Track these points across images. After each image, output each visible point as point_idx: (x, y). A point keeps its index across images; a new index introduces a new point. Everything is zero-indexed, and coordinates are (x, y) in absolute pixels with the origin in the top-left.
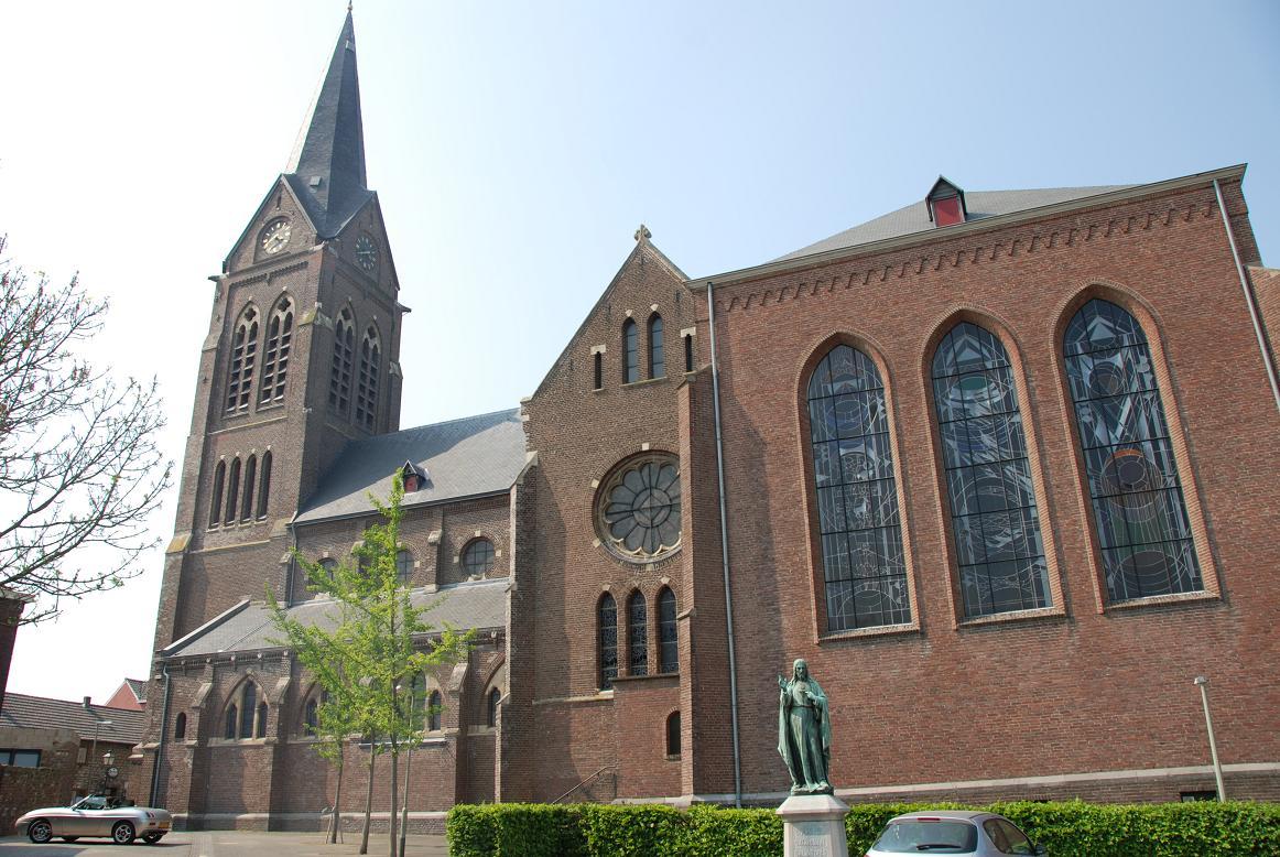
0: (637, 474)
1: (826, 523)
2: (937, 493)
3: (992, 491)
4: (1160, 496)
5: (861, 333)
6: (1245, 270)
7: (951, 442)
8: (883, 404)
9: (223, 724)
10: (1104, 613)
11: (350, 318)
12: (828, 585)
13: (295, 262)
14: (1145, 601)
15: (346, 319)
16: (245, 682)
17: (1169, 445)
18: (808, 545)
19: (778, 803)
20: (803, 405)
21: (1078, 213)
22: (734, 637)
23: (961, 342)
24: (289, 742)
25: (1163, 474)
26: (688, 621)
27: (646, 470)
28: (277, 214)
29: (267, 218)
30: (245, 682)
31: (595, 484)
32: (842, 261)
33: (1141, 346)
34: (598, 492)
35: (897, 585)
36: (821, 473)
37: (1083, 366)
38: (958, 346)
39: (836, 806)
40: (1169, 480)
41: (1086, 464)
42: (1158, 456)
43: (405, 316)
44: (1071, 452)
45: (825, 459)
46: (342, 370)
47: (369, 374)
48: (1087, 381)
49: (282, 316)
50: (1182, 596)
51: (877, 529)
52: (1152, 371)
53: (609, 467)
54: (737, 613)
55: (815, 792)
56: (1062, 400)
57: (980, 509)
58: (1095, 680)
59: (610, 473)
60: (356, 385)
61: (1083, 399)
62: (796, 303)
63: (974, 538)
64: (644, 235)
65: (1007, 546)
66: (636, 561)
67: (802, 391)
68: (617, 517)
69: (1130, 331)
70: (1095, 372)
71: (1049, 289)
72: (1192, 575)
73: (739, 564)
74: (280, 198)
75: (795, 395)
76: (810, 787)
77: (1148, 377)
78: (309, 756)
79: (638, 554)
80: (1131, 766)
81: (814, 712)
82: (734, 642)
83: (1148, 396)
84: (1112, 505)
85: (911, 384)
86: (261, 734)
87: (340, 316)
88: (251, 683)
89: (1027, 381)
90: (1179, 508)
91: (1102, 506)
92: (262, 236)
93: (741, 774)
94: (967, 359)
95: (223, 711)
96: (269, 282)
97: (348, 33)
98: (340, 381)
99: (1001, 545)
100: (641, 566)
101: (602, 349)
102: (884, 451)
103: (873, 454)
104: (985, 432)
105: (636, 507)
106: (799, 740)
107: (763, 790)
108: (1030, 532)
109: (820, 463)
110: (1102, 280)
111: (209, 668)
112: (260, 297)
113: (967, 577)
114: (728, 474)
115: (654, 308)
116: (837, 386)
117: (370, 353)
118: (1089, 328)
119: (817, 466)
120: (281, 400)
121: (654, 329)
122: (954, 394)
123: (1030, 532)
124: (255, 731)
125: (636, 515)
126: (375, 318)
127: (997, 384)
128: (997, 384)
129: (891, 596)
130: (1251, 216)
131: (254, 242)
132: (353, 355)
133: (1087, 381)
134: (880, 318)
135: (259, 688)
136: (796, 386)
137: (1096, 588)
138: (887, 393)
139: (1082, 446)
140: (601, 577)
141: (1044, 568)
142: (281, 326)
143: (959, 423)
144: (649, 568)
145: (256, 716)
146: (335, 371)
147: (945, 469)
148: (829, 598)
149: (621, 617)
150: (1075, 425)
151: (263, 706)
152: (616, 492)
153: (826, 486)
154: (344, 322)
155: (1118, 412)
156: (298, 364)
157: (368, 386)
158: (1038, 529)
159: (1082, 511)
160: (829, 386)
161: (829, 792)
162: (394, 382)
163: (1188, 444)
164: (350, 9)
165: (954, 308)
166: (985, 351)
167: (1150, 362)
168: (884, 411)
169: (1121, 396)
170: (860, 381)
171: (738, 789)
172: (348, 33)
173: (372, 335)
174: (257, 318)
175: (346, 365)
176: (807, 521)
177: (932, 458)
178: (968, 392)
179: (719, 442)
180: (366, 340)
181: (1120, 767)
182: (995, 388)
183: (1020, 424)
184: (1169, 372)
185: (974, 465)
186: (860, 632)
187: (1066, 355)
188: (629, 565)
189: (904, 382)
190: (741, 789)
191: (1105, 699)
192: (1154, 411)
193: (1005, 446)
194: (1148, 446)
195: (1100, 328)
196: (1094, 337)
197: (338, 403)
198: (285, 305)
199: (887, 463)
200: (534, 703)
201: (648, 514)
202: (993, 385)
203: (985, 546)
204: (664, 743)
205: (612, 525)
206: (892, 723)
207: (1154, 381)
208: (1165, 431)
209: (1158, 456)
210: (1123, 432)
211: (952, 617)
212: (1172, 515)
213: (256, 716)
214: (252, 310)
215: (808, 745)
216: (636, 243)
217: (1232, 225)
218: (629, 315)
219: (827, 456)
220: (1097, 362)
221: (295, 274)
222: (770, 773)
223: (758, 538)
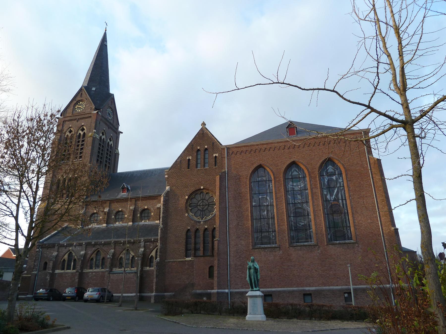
0: (199, 195)
1: (255, 216)
2: (285, 210)
3: (300, 210)
4: (343, 215)
6: (368, 157)
7: (289, 196)
8: (272, 185)
9: (60, 265)
10: (327, 245)
11: (104, 135)
12: (255, 233)
13: (87, 116)
14: (338, 242)
16: (69, 252)
17: (346, 202)
18: (250, 222)
19: (247, 292)
20: (250, 183)
22: (229, 246)
23: (294, 169)
24: (83, 272)
25: (344, 209)
27: (202, 195)
28: (80, 99)
29: (77, 100)
30: (69, 252)
31: (187, 197)
33: (340, 174)
34: (187, 200)
35: (273, 234)
36: (254, 202)
37: (325, 179)
38: (292, 171)
39: (261, 294)
40: (345, 211)
41: (324, 205)
42: (343, 204)
43: (121, 135)
44: (321, 202)
45: (255, 199)
46: (101, 152)
47: (109, 153)
48: (326, 183)
49: (82, 133)
50: (347, 241)
51: (269, 219)
52: (343, 181)
53: (191, 193)
54: (230, 239)
55: (256, 290)
56: (319, 188)
57: (297, 215)
58: (324, 262)
59: (191, 194)
60: (105, 157)
61: (325, 187)
62: (249, 155)
63: (294, 223)
64: (204, 124)
65: (303, 225)
66: (198, 220)
67: (250, 179)
68: (193, 207)
69: (338, 170)
70: (328, 180)
71: (317, 157)
72: (350, 236)
73: (231, 226)
74: (82, 94)
75: (248, 181)
76: (255, 289)
77: (342, 183)
78: (90, 276)
79: (198, 218)
82: (229, 247)
83: (342, 188)
84: (331, 216)
85: (279, 180)
86: (73, 269)
87: (101, 134)
88: (71, 252)
89: (310, 182)
90: (347, 218)
91: (328, 217)
93: (230, 284)
94: (295, 174)
95: (61, 261)
96: (77, 121)
97: (104, 40)
98: (100, 155)
99: (301, 225)
100: (200, 222)
102: (271, 198)
103: (268, 198)
104: (299, 194)
105: (198, 204)
106: (252, 277)
107: (236, 289)
108: (309, 222)
109: (254, 200)
110: (331, 156)
111: (56, 247)
112: (73, 126)
113: (292, 233)
114: (229, 201)
115: (206, 147)
116: (260, 179)
118: (327, 169)
119: (253, 200)
121: (206, 153)
122: (291, 183)
123: (309, 222)
124: (72, 268)
126: (112, 135)
127: (302, 182)
128: (302, 182)
129: (272, 237)
131: (72, 108)
132: (104, 147)
133: (326, 183)
134: (272, 161)
135: (74, 254)
136: (248, 178)
137: (325, 238)
138: (273, 182)
139: (324, 200)
141: (312, 232)
142: (81, 136)
143: (292, 191)
144: (202, 223)
145: (72, 263)
146: (99, 152)
147: (287, 204)
148: (255, 236)
149: (193, 237)
150: (322, 194)
151: (75, 260)
152: (193, 200)
153: (255, 206)
154: (110, 142)
155: (334, 192)
156: (87, 150)
157: (108, 157)
158: (311, 221)
159: (323, 218)
160: (258, 179)
162: (116, 156)
163: (351, 202)
164: (106, 30)
165: (292, 160)
166: (300, 172)
167: (343, 179)
168: (272, 187)
169: (334, 187)
170: (266, 178)
171: (229, 288)
172: (104, 40)
173: (110, 140)
175: (102, 150)
176: (250, 215)
177: (284, 201)
178: (295, 183)
179: (227, 192)
180: (109, 142)
181: (329, 286)
182: (302, 183)
183: (308, 193)
184: (347, 182)
185: (295, 203)
186: (263, 246)
187: (321, 175)
188: (196, 222)
189: (278, 179)
190: (230, 288)
191: (326, 268)
192: (343, 192)
193: (304, 198)
194: (340, 201)
195: (330, 169)
196: (329, 171)
198: (83, 130)
199: (272, 201)
200: (166, 261)
201: (202, 207)
202: (301, 182)
203: (297, 225)
204: (208, 275)
205: (191, 210)
206: (271, 271)
207: (343, 184)
208: (345, 198)
209: (343, 204)
210: (335, 197)
211: (287, 244)
212: (346, 220)
213: (72, 263)
214: (71, 130)
215: (254, 278)
216: (201, 127)
218: (198, 148)
219: (256, 198)
220: (329, 178)
221: (87, 120)
222: (238, 284)
223: (236, 219)
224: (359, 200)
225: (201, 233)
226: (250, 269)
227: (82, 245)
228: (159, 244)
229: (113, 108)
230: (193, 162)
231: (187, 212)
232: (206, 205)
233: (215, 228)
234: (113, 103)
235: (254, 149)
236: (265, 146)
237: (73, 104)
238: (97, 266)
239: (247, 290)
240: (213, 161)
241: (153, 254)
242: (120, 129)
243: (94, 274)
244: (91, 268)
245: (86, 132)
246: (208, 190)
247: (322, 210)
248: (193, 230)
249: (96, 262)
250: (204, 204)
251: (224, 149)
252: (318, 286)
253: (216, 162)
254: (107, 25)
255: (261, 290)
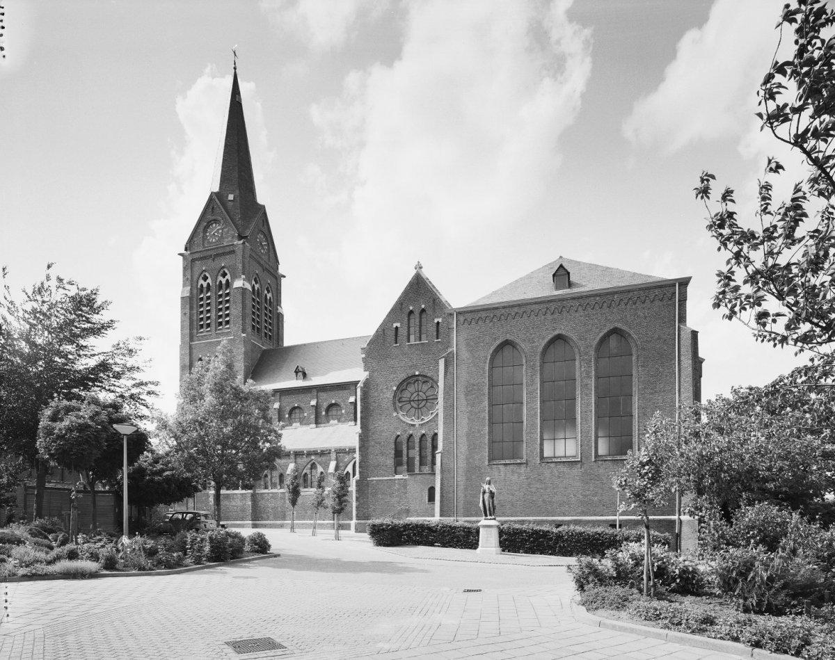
2: (539, 411)
5: (517, 341)
10: (595, 461)
13: (228, 250)
15: (256, 283)
19: (478, 521)
21: (616, 293)
26: (440, 455)
27: (416, 384)
32: (513, 306)
39: (497, 523)
59: (401, 384)
66: (412, 423)
76: (489, 517)
80: (595, 515)
81: (492, 495)
87: (253, 282)
92: (205, 230)
101: (398, 325)
110: (619, 325)
115: (423, 306)
117: (268, 302)
120: (228, 328)
125: (412, 403)
130: (687, 301)
134: (525, 334)
136: (488, 361)
140: (397, 429)
161: (495, 519)
164: (235, 68)
165: (556, 332)
174: (209, 280)
176: (487, 418)
197: (256, 329)
214: (205, 275)
217: (679, 305)
224: (651, 396)
225: (417, 440)
226: (484, 493)
227: (289, 456)
228: (357, 455)
229: (266, 232)
230: (402, 332)
231: (395, 410)
232: (424, 400)
233: (436, 434)
234: (265, 224)
235: (499, 315)
236: (516, 310)
237: (202, 227)
238: (274, 486)
239: (479, 518)
240: (433, 329)
241: (349, 469)
242: (281, 270)
243: (271, 495)
244: (266, 488)
245: (229, 279)
246: (426, 376)
247: (593, 411)
248: (405, 437)
249: (271, 480)
250: (420, 398)
251: (451, 315)
252: (576, 516)
253: (438, 331)
254: (235, 55)
255: (497, 518)
